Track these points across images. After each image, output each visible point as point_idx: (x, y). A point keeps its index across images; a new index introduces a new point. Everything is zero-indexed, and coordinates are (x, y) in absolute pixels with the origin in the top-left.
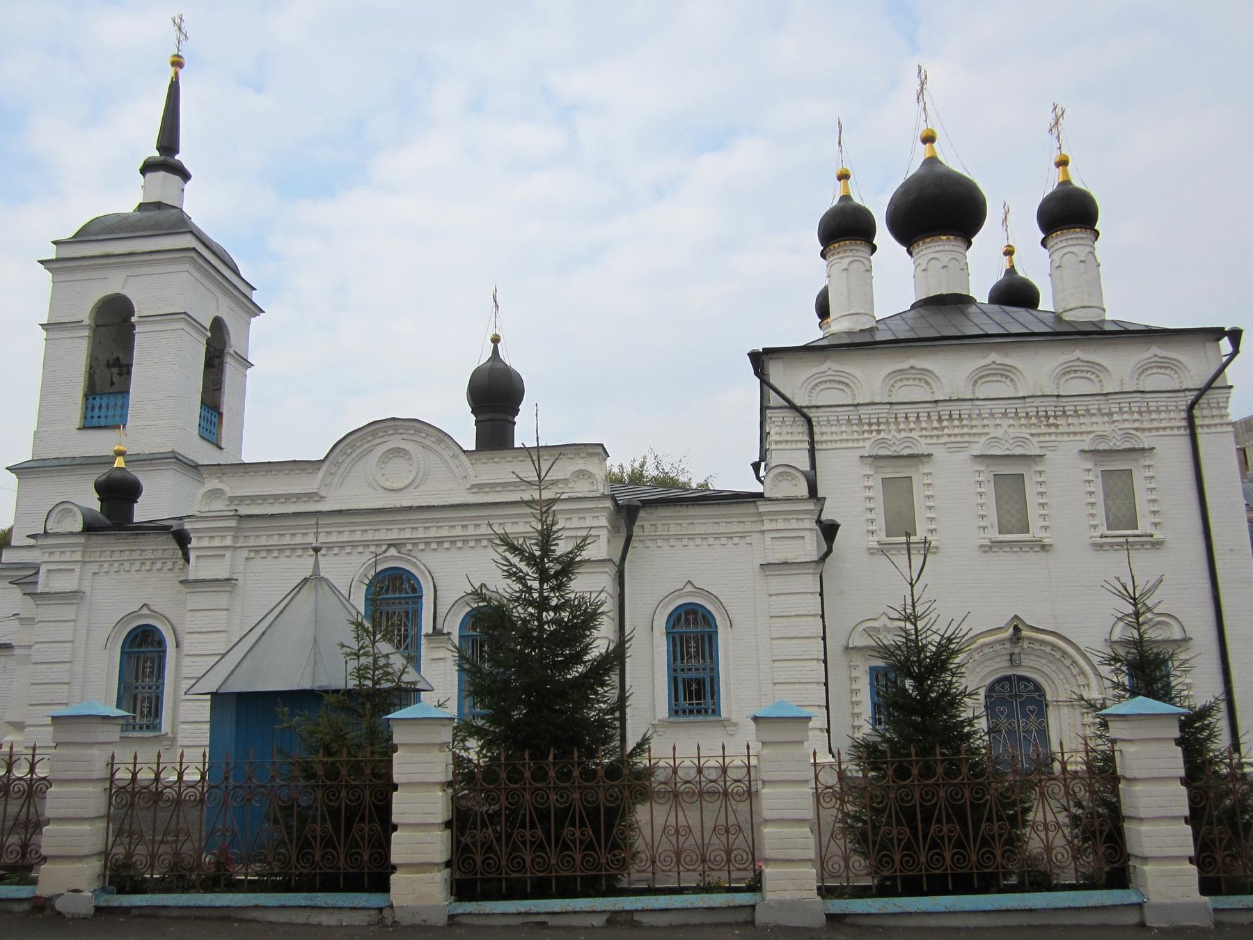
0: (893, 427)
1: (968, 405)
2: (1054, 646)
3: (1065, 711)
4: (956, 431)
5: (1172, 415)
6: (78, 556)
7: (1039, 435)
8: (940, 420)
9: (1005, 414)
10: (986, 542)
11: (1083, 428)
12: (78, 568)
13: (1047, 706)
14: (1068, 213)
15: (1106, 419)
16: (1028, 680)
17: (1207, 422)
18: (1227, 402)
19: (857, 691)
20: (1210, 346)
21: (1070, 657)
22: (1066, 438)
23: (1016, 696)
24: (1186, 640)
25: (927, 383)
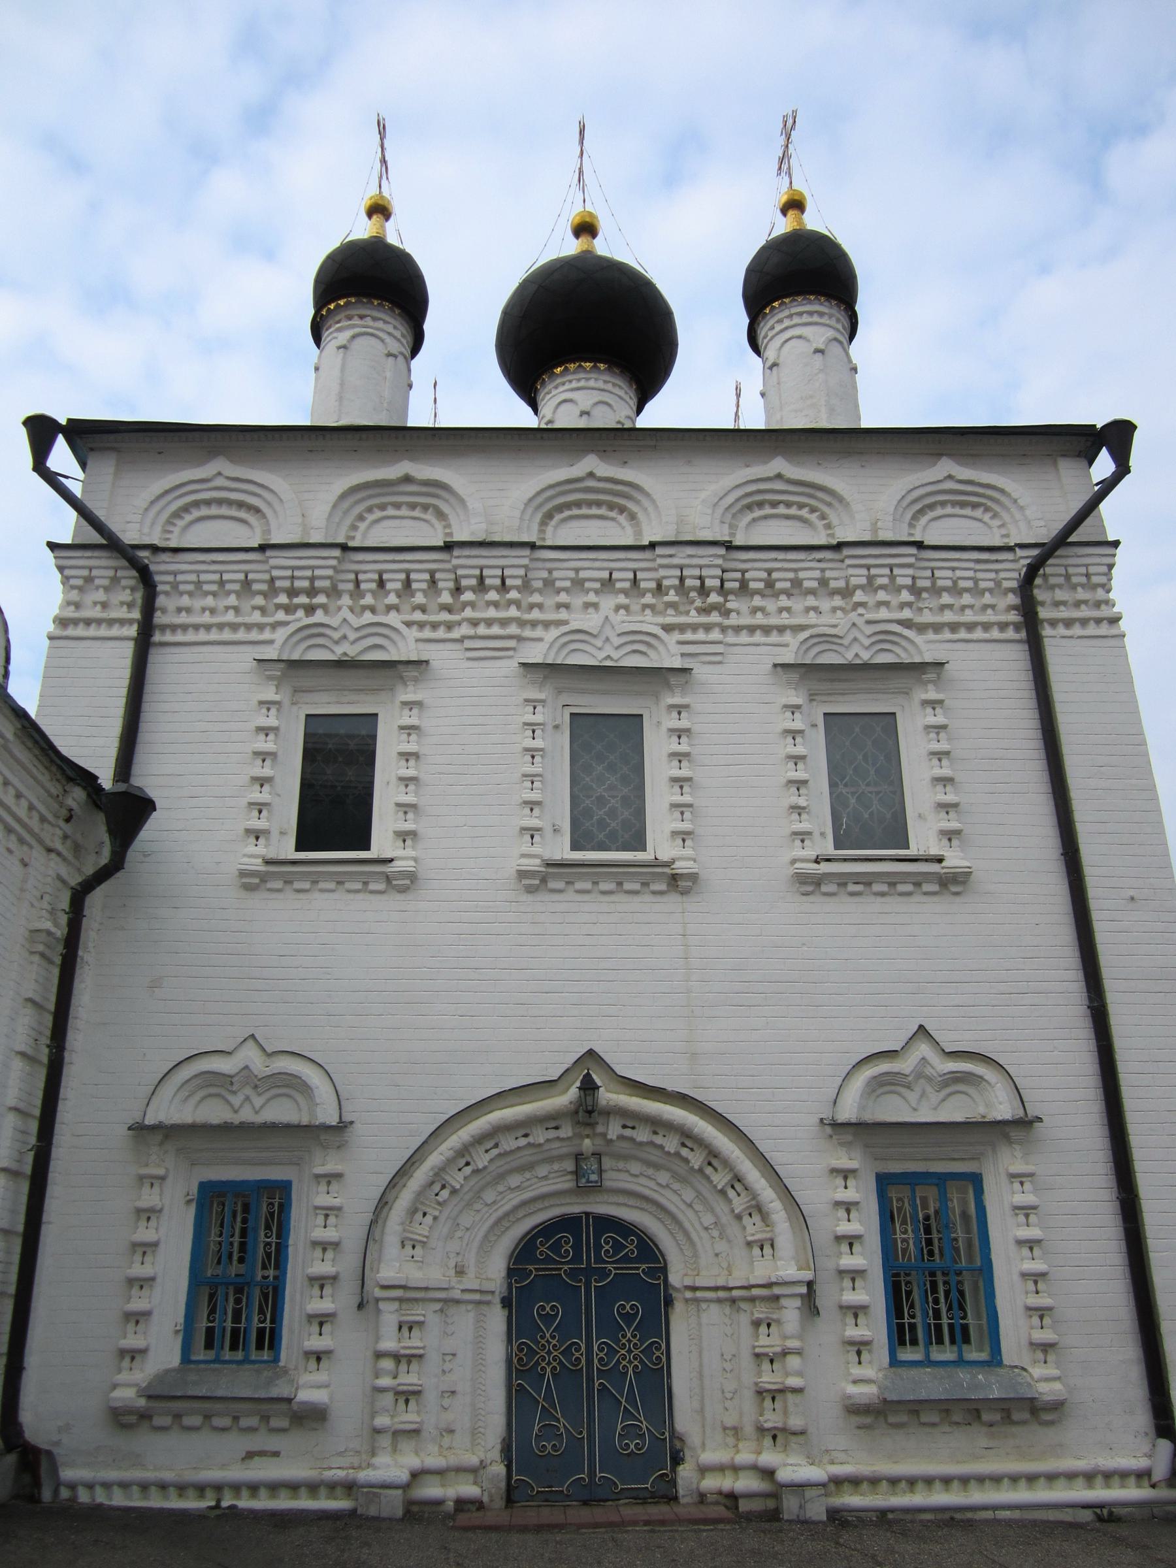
0: (346, 600)
1: (522, 557)
2: (687, 1136)
3: (714, 1314)
4: (492, 613)
5: (987, 599)
7: (682, 628)
8: (458, 590)
9: (608, 583)
10: (534, 864)
11: (785, 619)
13: (669, 1302)
14: (802, 276)
15: (838, 601)
16: (623, 1228)
17: (1064, 613)
18: (1108, 575)
19: (146, 1249)
20: (1068, 469)
21: (727, 1164)
22: (744, 638)
23: (589, 1272)
24: (1025, 1123)
25: (441, 515)
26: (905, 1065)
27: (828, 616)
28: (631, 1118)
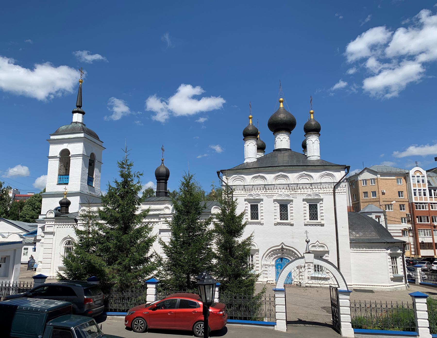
2: (293, 252)
6: (53, 223)
7: (292, 194)
9: (283, 188)
10: (276, 222)
12: (53, 226)
15: (311, 190)
24: (258, 251)
26: (315, 245)
27: (309, 192)
28: (287, 249)
